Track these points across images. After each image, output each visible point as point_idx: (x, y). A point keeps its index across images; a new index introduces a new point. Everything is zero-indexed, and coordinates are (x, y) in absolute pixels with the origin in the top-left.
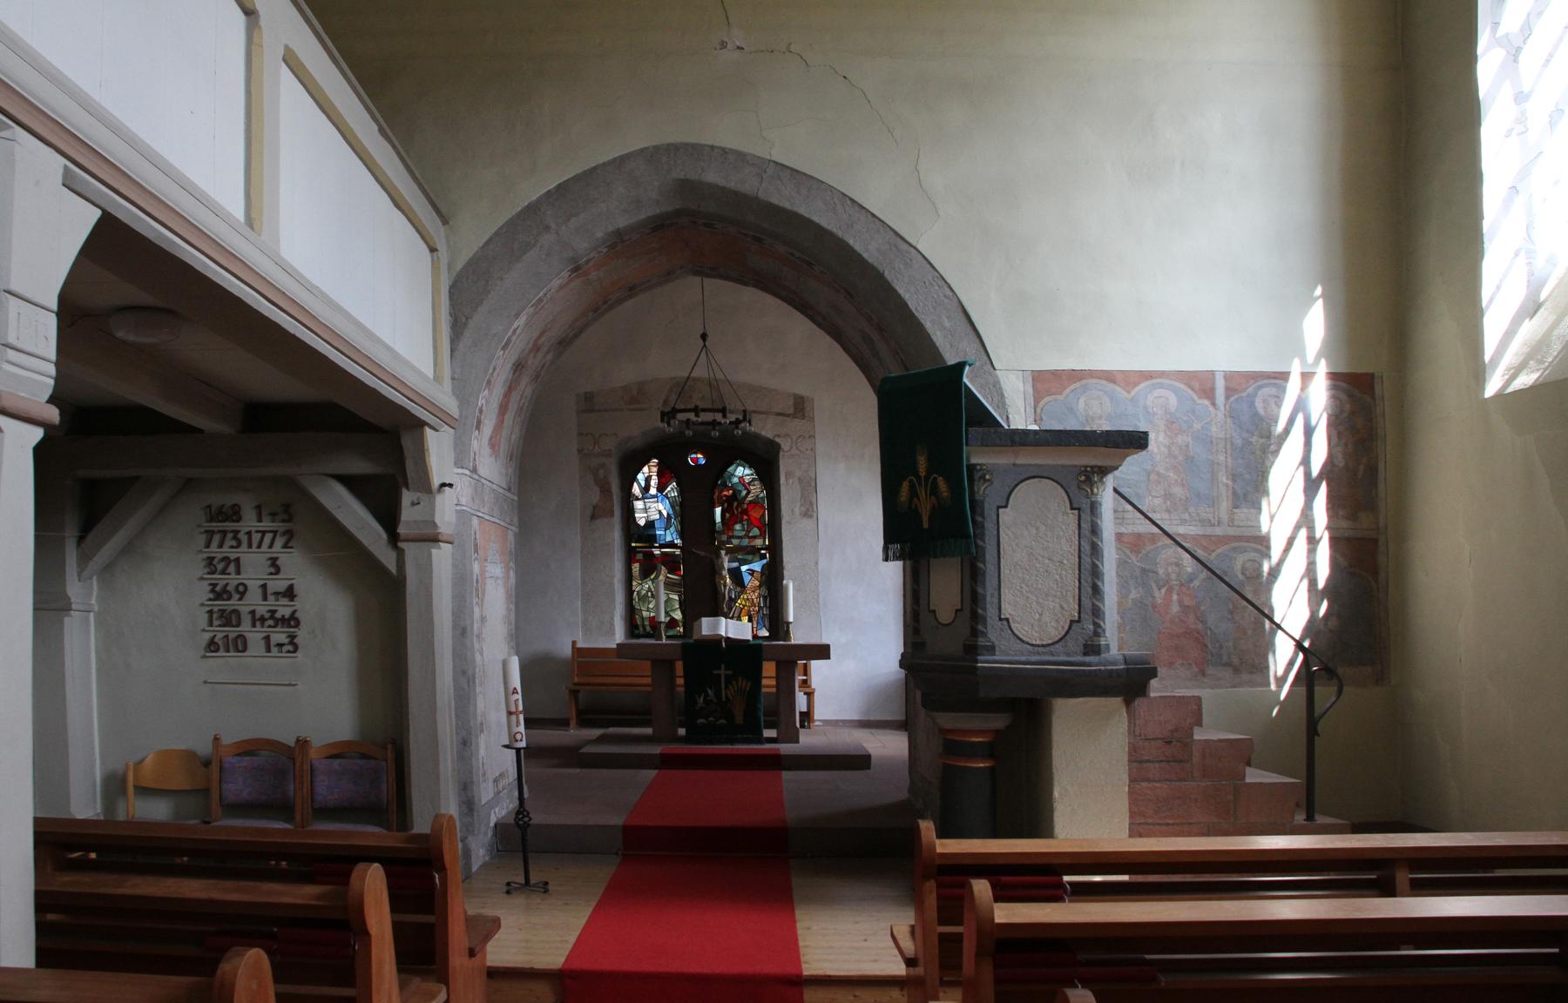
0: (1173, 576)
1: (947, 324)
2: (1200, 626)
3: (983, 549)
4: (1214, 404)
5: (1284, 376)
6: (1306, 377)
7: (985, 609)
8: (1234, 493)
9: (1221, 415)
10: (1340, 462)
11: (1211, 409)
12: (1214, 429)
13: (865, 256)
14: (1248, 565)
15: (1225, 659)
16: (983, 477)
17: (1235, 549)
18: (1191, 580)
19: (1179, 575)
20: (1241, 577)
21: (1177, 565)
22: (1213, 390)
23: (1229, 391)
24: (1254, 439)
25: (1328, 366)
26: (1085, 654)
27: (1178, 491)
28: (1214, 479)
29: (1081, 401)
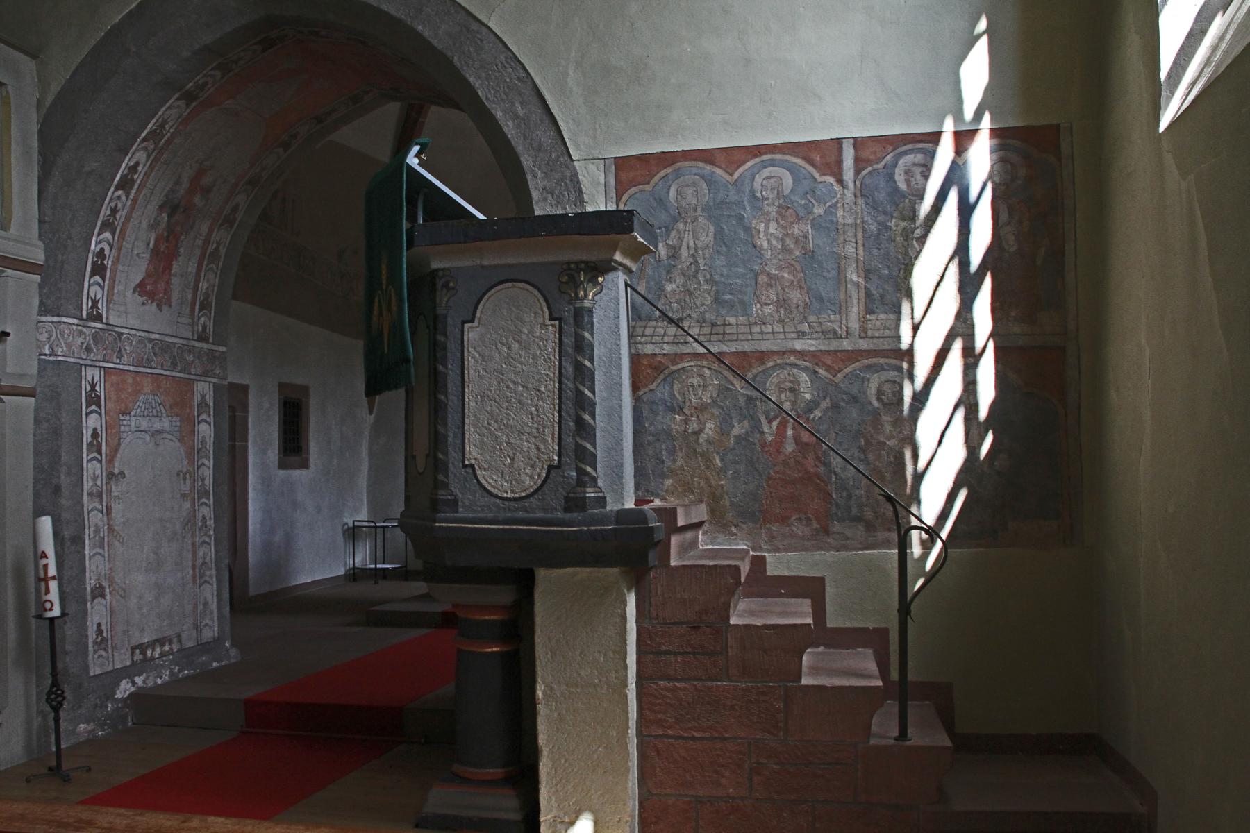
1: (520, 112)
2: (821, 469)
3: (445, 376)
4: (840, 181)
5: (935, 137)
6: (963, 139)
7: (446, 453)
8: (868, 294)
9: (849, 195)
10: (1011, 245)
11: (837, 187)
12: (840, 213)
13: (435, 42)
15: (854, 511)
16: (446, 285)
17: (869, 367)
18: (811, 410)
19: (794, 403)
20: (876, 404)
21: (792, 390)
22: (839, 162)
23: (859, 163)
24: (892, 224)
25: (992, 120)
26: (567, 510)
27: (795, 296)
28: (841, 279)
29: (673, 190)
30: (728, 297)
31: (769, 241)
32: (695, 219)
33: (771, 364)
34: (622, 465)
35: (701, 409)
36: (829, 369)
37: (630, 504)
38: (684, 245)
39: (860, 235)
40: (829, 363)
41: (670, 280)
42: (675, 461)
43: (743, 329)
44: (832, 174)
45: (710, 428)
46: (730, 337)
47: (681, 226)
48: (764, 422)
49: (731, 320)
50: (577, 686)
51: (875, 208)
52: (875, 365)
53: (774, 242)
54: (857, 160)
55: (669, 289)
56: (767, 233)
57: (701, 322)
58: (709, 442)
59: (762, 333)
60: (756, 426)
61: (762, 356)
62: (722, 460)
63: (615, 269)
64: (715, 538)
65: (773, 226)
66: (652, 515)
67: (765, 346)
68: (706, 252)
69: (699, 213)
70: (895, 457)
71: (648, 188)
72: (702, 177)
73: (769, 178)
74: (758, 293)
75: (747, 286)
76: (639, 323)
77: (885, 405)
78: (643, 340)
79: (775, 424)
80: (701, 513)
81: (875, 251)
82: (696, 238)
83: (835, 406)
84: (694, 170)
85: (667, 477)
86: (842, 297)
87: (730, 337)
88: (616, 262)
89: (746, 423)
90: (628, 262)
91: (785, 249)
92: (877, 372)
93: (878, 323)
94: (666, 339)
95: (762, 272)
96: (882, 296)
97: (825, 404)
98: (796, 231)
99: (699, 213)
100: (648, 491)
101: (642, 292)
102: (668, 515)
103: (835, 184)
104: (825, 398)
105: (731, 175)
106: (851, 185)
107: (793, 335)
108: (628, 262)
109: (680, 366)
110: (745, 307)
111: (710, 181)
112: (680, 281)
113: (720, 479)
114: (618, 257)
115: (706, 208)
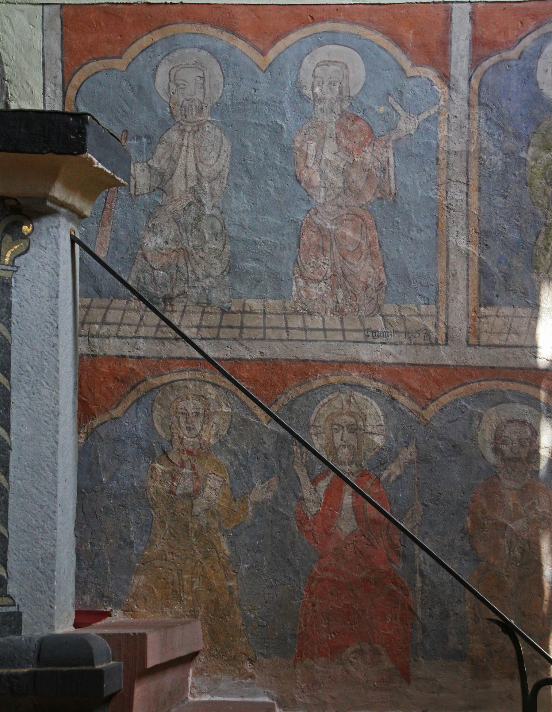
0: (344, 454)
4: (445, 77)
8: (484, 272)
9: (459, 102)
11: (439, 87)
12: (443, 132)
14: (509, 431)
15: (453, 641)
17: (480, 395)
18: (383, 464)
19: (356, 451)
20: (492, 458)
21: (353, 429)
22: (445, 44)
23: (480, 46)
24: (528, 154)
27: (363, 269)
28: (439, 245)
29: (163, 70)
30: (250, 265)
31: (322, 174)
32: (198, 127)
33: (319, 382)
34: (53, 556)
35: (198, 453)
36: (414, 394)
37: (65, 626)
38: (179, 170)
39: (474, 173)
40: (415, 385)
41: (153, 230)
42: (151, 542)
43: (275, 321)
44: (433, 63)
45: (213, 490)
46: (254, 333)
47: (174, 136)
48: (305, 481)
49: (256, 304)
50: (182, 413)
51: (500, 127)
52: (492, 392)
53: (331, 175)
54: (476, 42)
55: (151, 246)
56: (322, 160)
57: (205, 305)
58: (210, 511)
59: (305, 329)
60: (292, 488)
61: (305, 369)
62: (232, 544)
63: (52, 213)
64: (216, 681)
65: (330, 147)
66: (100, 647)
67: (312, 351)
68: (216, 185)
69: (206, 116)
70: (523, 551)
71: (119, 64)
72: (214, 54)
73: (328, 63)
74: (302, 259)
75: (283, 248)
76: (97, 301)
77: (506, 460)
78: (104, 330)
79: (323, 485)
80: (192, 637)
81: (498, 201)
82: (199, 161)
83: (423, 459)
84: (201, 41)
85: (137, 572)
86: (441, 275)
87: (254, 333)
88: (55, 201)
89: (274, 481)
90: (76, 201)
91: (348, 188)
92: (495, 404)
93: (499, 322)
94: (143, 332)
95: (309, 225)
96: (506, 277)
97: (408, 454)
98: (368, 157)
99: (206, 116)
100: (102, 596)
101: (102, 255)
102: (131, 647)
103: (437, 82)
104: (407, 445)
105: (263, 54)
106: (463, 85)
107: (360, 336)
108: (76, 201)
109: (166, 379)
110: (279, 282)
111: (226, 64)
112: (170, 231)
113: (228, 577)
114: (58, 192)
115: (218, 109)
